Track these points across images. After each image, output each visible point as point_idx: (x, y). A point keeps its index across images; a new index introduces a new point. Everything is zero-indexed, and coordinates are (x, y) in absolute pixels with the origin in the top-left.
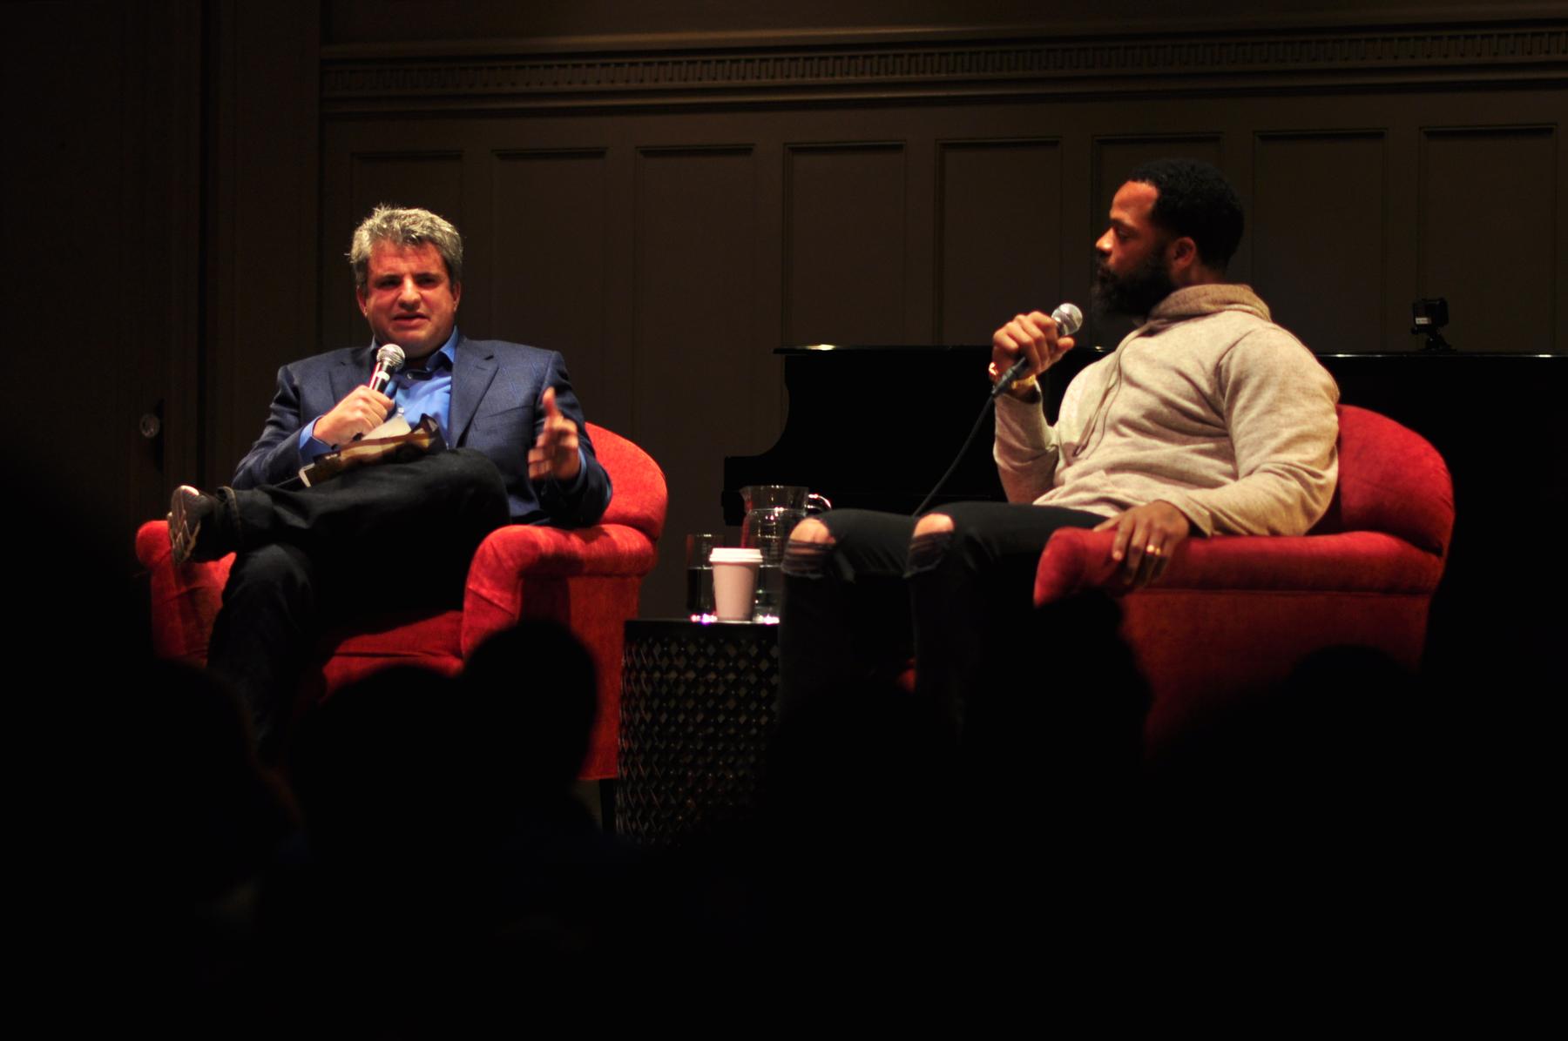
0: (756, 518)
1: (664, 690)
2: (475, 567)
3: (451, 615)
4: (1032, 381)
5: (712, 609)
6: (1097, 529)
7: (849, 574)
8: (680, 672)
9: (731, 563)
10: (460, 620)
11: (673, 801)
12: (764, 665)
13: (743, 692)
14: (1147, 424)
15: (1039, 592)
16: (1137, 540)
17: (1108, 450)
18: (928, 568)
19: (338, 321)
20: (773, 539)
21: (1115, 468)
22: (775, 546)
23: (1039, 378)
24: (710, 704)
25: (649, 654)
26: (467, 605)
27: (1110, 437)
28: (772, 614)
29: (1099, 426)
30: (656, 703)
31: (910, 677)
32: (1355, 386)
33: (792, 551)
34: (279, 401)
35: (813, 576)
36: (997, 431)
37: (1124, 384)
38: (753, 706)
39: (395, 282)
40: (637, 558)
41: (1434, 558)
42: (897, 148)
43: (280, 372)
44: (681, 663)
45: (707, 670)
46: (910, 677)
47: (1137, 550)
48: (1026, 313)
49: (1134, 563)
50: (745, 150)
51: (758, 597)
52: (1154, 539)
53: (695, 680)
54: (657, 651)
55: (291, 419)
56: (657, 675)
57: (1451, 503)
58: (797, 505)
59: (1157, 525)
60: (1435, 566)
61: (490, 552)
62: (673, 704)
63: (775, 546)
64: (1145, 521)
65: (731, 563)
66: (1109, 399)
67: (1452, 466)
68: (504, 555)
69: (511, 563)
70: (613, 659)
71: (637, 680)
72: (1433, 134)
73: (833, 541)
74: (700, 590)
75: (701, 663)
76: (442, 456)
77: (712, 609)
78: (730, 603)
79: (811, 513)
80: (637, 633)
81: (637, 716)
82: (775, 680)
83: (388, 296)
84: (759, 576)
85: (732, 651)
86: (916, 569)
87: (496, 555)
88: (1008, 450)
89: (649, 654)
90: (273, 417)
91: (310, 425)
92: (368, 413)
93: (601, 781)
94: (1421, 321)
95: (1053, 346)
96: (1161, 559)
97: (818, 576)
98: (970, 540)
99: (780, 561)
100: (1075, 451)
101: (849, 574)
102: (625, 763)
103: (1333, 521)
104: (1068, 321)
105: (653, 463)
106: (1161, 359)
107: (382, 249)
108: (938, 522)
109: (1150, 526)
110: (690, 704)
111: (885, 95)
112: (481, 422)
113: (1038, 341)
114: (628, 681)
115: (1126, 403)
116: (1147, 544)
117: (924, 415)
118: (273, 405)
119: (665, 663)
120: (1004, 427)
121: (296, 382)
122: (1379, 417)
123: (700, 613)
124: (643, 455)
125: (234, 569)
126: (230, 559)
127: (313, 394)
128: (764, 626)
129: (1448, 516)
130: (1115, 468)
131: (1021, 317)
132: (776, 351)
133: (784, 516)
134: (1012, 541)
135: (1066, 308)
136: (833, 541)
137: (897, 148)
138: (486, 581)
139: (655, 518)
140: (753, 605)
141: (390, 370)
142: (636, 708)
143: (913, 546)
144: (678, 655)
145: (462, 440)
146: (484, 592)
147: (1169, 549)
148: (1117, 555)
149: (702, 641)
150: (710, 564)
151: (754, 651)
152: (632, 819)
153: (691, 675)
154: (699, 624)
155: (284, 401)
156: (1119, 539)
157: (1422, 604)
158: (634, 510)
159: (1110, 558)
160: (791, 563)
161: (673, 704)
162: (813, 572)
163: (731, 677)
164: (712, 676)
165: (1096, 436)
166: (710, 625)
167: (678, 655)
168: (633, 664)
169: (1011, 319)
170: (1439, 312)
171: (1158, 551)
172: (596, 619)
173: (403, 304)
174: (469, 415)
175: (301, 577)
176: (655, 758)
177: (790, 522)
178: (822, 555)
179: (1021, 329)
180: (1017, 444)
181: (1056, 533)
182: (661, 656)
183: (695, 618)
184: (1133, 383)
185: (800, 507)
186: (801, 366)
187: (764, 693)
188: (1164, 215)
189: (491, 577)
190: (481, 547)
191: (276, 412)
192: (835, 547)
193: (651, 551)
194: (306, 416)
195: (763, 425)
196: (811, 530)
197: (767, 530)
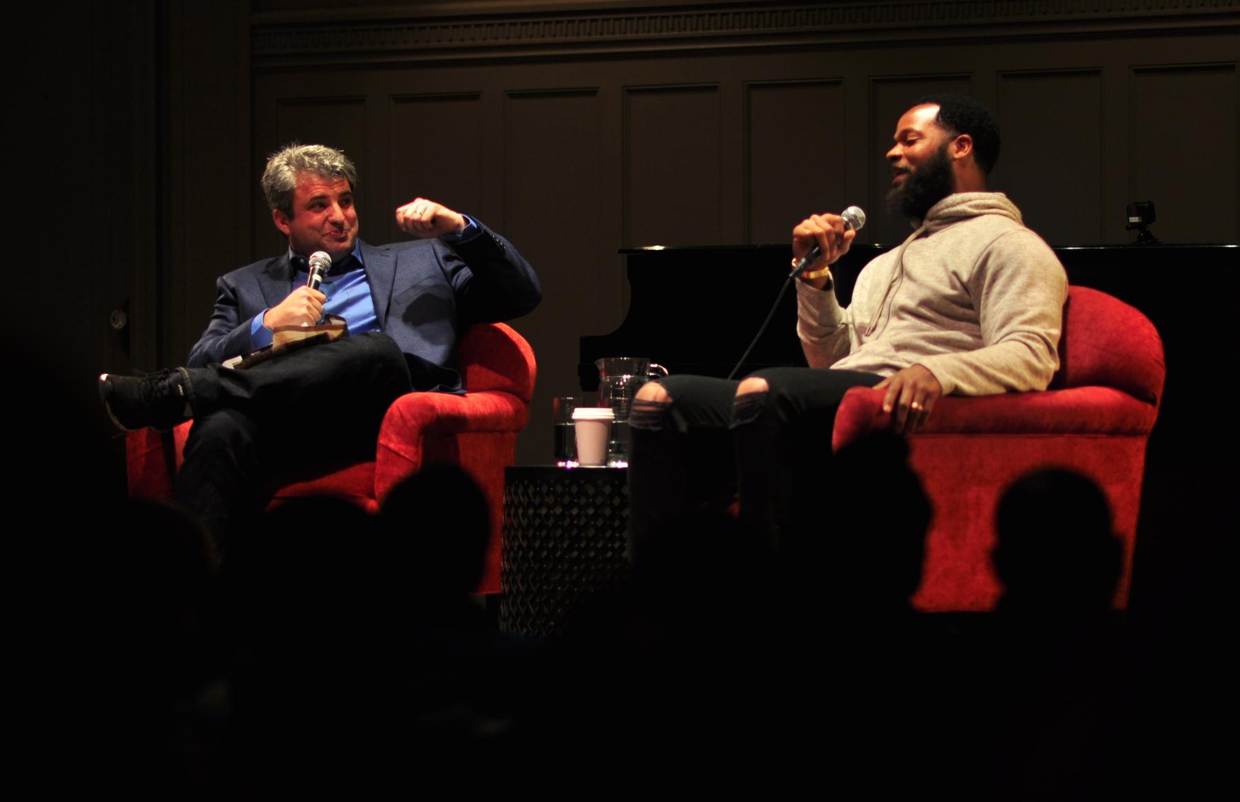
1: (537, 522)
2: (384, 425)
3: (367, 465)
4: (827, 272)
5: (575, 457)
6: (876, 388)
7: (683, 427)
8: (550, 507)
9: (589, 419)
10: (374, 469)
11: (546, 610)
12: (617, 501)
13: (600, 523)
14: (923, 311)
15: (836, 438)
16: (904, 399)
17: (893, 332)
18: (749, 421)
20: (622, 400)
21: (899, 347)
23: (832, 268)
24: (574, 532)
25: (525, 493)
26: (379, 456)
27: (894, 322)
28: (623, 460)
29: (885, 311)
30: (531, 533)
31: (735, 508)
32: (1080, 269)
33: (638, 408)
34: (221, 302)
35: (654, 429)
36: (799, 312)
37: (905, 279)
38: (609, 533)
39: (321, 203)
41: (1150, 407)
42: (714, 88)
43: (219, 281)
44: (550, 500)
45: (571, 505)
46: (735, 508)
47: (904, 407)
48: (820, 214)
49: (903, 418)
50: (592, 92)
51: (611, 446)
52: (917, 397)
53: (563, 513)
54: (531, 491)
55: (232, 314)
56: (531, 511)
59: (921, 385)
60: (1150, 414)
61: (397, 414)
64: (910, 382)
65: (589, 419)
66: (893, 290)
68: (408, 417)
69: (413, 423)
70: (498, 496)
72: (1138, 72)
73: (670, 400)
74: (565, 442)
75: (567, 500)
77: (575, 457)
78: (588, 452)
79: (652, 378)
80: (513, 476)
82: (626, 512)
83: (317, 218)
84: (611, 429)
86: (739, 422)
88: (808, 328)
89: (525, 493)
90: (216, 313)
91: (261, 315)
93: (487, 596)
94: (1134, 219)
95: (840, 236)
96: (924, 414)
97: (658, 428)
98: (782, 399)
99: (626, 418)
100: (863, 331)
101: (683, 427)
102: (507, 581)
103: (1059, 381)
104: (854, 220)
106: (933, 258)
108: (755, 384)
109: (914, 387)
110: (559, 533)
111: (702, 47)
113: (828, 233)
114: (509, 515)
115: (905, 296)
116: (912, 401)
117: (741, 300)
119: (537, 501)
120: (805, 312)
122: (1104, 295)
123: (565, 460)
125: (192, 431)
126: (188, 425)
127: (250, 296)
128: (616, 469)
129: (1160, 374)
130: (899, 347)
131: (815, 216)
132: (620, 252)
134: (815, 398)
135: (852, 210)
136: (670, 400)
137: (714, 88)
138: (393, 437)
140: (607, 453)
141: (321, 273)
142: (516, 537)
143: (736, 404)
144: (548, 493)
146: (392, 446)
147: (930, 405)
148: (887, 408)
149: (567, 482)
150: (573, 421)
151: (608, 490)
153: (558, 511)
154: (564, 468)
155: (226, 301)
156: (889, 396)
157: (1141, 443)
159: (881, 411)
160: (635, 418)
161: (544, 533)
162: (654, 425)
164: (575, 512)
165: (883, 320)
166: (572, 469)
167: (548, 493)
169: (808, 217)
170: (1147, 213)
171: (921, 408)
172: (483, 463)
173: (334, 223)
175: (246, 437)
176: (531, 576)
177: (635, 386)
178: (662, 412)
179: (814, 224)
180: (814, 323)
181: (850, 391)
182: (535, 494)
183: (561, 464)
184: (910, 278)
185: (643, 374)
186: (640, 263)
187: (617, 523)
188: (943, 120)
189: (398, 434)
190: (389, 410)
191: (219, 309)
192: (672, 405)
195: (610, 309)
196: (653, 391)
197: (617, 393)
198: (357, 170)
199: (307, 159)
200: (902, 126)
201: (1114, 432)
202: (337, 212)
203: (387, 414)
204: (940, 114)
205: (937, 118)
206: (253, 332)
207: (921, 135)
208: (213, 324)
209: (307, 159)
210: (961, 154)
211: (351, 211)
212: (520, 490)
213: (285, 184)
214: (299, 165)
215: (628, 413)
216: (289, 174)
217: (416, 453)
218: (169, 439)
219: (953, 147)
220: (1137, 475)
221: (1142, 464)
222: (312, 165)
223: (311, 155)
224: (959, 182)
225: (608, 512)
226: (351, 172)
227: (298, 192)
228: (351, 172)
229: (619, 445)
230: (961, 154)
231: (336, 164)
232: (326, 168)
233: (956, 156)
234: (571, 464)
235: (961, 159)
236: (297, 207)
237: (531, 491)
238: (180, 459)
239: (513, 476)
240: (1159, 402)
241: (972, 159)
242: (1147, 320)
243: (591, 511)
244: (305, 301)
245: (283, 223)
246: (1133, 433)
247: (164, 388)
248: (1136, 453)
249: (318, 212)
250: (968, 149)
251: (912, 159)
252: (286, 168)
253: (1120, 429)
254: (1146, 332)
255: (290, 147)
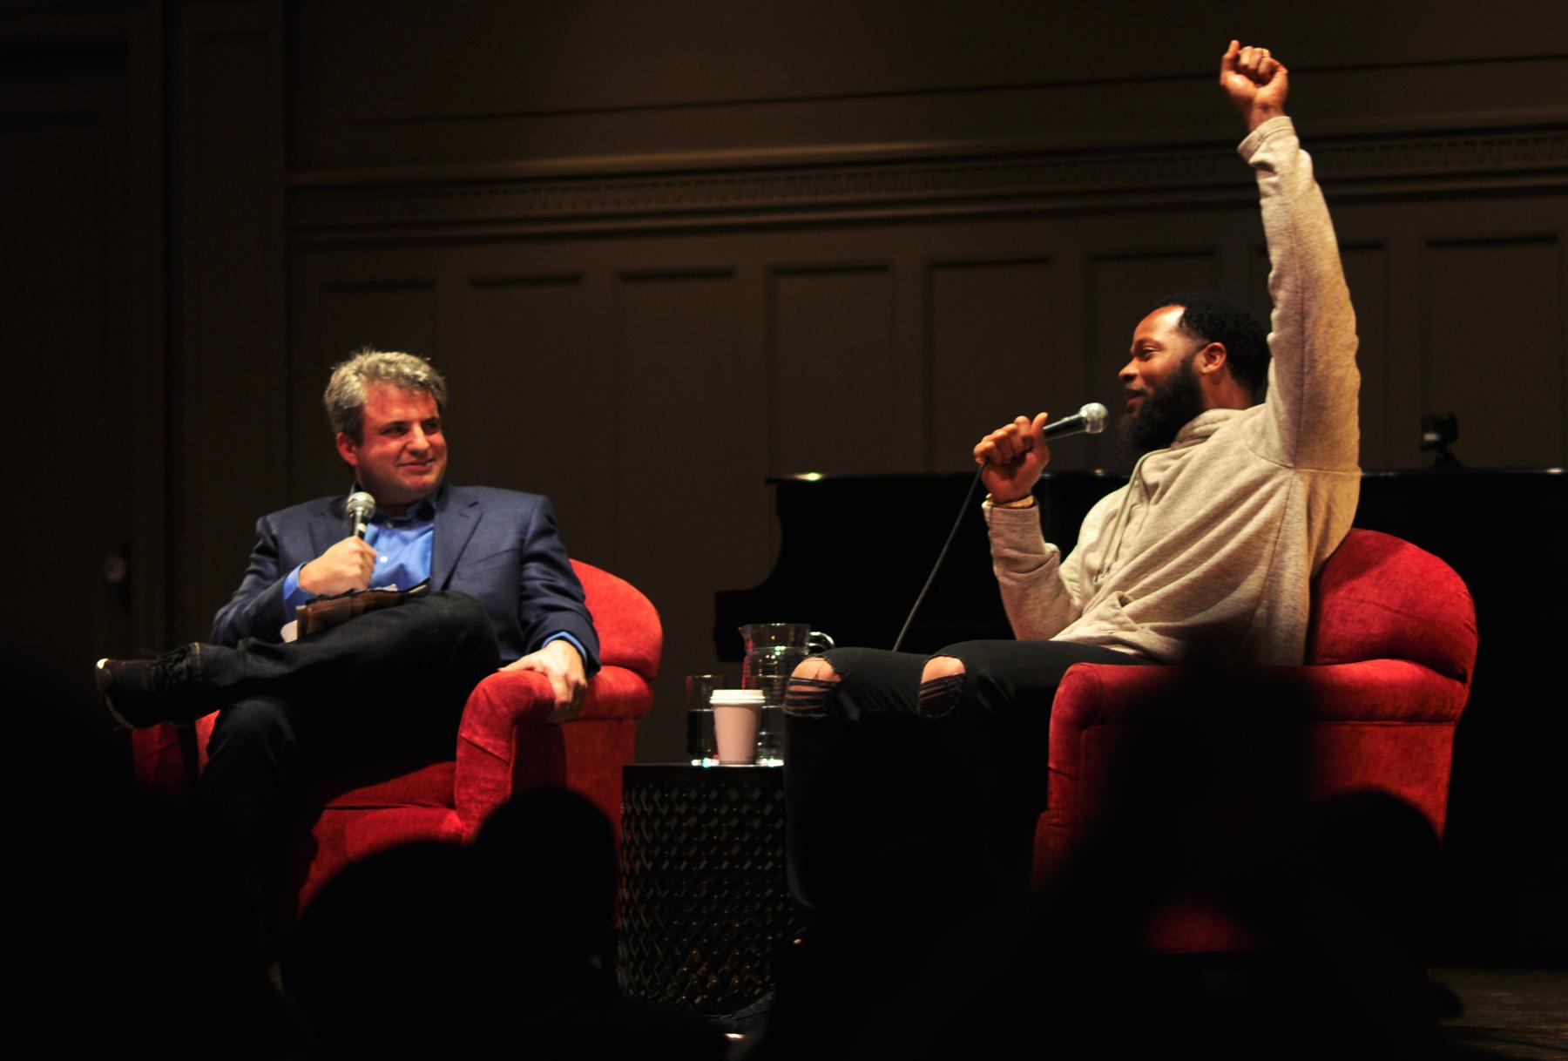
0: (758, 657)
2: (467, 713)
3: (444, 765)
5: (713, 753)
9: (732, 704)
12: (768, 810)
13: (746, 837)
19: (317, 463)
22: (777, 686)
25: (649, 801)
26: (459, 753)
28: (776, 757)
33: (793, 688)
34: (259, 551)
39: (401, 428)
40: (633, 701)
41: (1458, 684)
43: (259, 522)
51: (760, 738)
55: (271, 568)
56: (657, 824)
57: (1474, 628)
58: (799, 642)
60: (1459, 694)
62: (674, 851)
63: (777, 686)
65: (732, 704)
67: (1473, 591)
68: (497, 702)
70: (617, 808)
71: (638, 828)
73: (837, 679)
74: (701, 734)
76: (427, 599)
78: (731, 746)
79: (814, 651)
80: (634, 778)
81: (638, 864)
82: (779, 795)
83: (394, 445)
84: (761, 717)
85: (734, 795)
87: (489, 701)
90: (253, 567)
92: (346, 561)
94: (1431, 437)
98: (982, 680)
99: (780, 701)
101: (854, 714)
105: (647, 602)
107: (383, 394)
108: (944, 666)
112: (464, 570)
114: (628, 828)
118: (253, 555)
121: (274, 532)
123: (701, 757)
124: (637, 594)
125: (217, 720)
126: (215, 714)
127: (292, 545)
128: (767, 769)
129: (1472, 642)
132: (769, 481)
133: (785, 655)
136: (837, 679)
139: (650, 659)
142: (637, 856)
145: (446, 585)
146: (477, 740)
150: (711, 706)
151: (756, 794)
152: (635, 972)
154: (700, 768)
155: (264, 550)
157: (1448, 731)
158: (629, 651)
160: (791, 703)
161: (674, 851)
162: (815, 711)
163: (734, 822)
166: (712, 769)
168: (633, 811)
170: (1448, 429)
172: (593, 773)
173: (414, 453)
174: (451, 564)
177: (792, 660)
178: (827, 693)
181: (1071, 669)
183: (695, 763)
185: (802, 645)
188: (1189, 324)
189: (485, 724)
191: (257, 562)
192: (839, 685)
193: (646, 693)
194: (285, 567)
195: (754, 557)
196: (815, 668)
197: (768, 669)
198: (447, 382)
199: (382, 366)
200: (1139, 335)
201: (1413, 718)
202: (420, 439)
203: (471, 699)
204: (1185, 317)
205: (1180, 324)
206: (287, 596)
207: (1159, 347)
208: (248, 580)
209: (382, 366)
210: (1212, 367)
211: (438, 438)
212: (643, 796)
213: (352, 399)
214: (373, 375)
215: (782, 696)
216: (358, 385)
217: (509, 749)
218: (190, 734)
219: (1200, 359)
220: (1443, 774)
221: (1448, 760)
222: (388, 374)
223: (389, 363)
224: (1211, 401)
225: (757, 824)
226: (437, 386)
227: (370, 411)
228: (437, 386)
229: (770, 737)
230: (1212, 367)
231: (418, 373)
232: (406, 377)
233: (1205, 370)
234: (708, 763)
235: (1211, 374)
236: (366, 430)
237: (656, 797)
238: (204, 758)
239: (634, 778)
240: (1469, 679)
241: (1227, 373)
242: (1453, 573)
243: (734, 822)
244: (358, 559)
245: (349, 450)
246: (1438, 719)
247: (181, 672)
248: (1441, 741)
249: (395, 438)
250: (1220, 360)
251: (1149, 378)
252: (354, 378)
253: (1419, 714)
254: (1453, 588)
255: (361, 352)
